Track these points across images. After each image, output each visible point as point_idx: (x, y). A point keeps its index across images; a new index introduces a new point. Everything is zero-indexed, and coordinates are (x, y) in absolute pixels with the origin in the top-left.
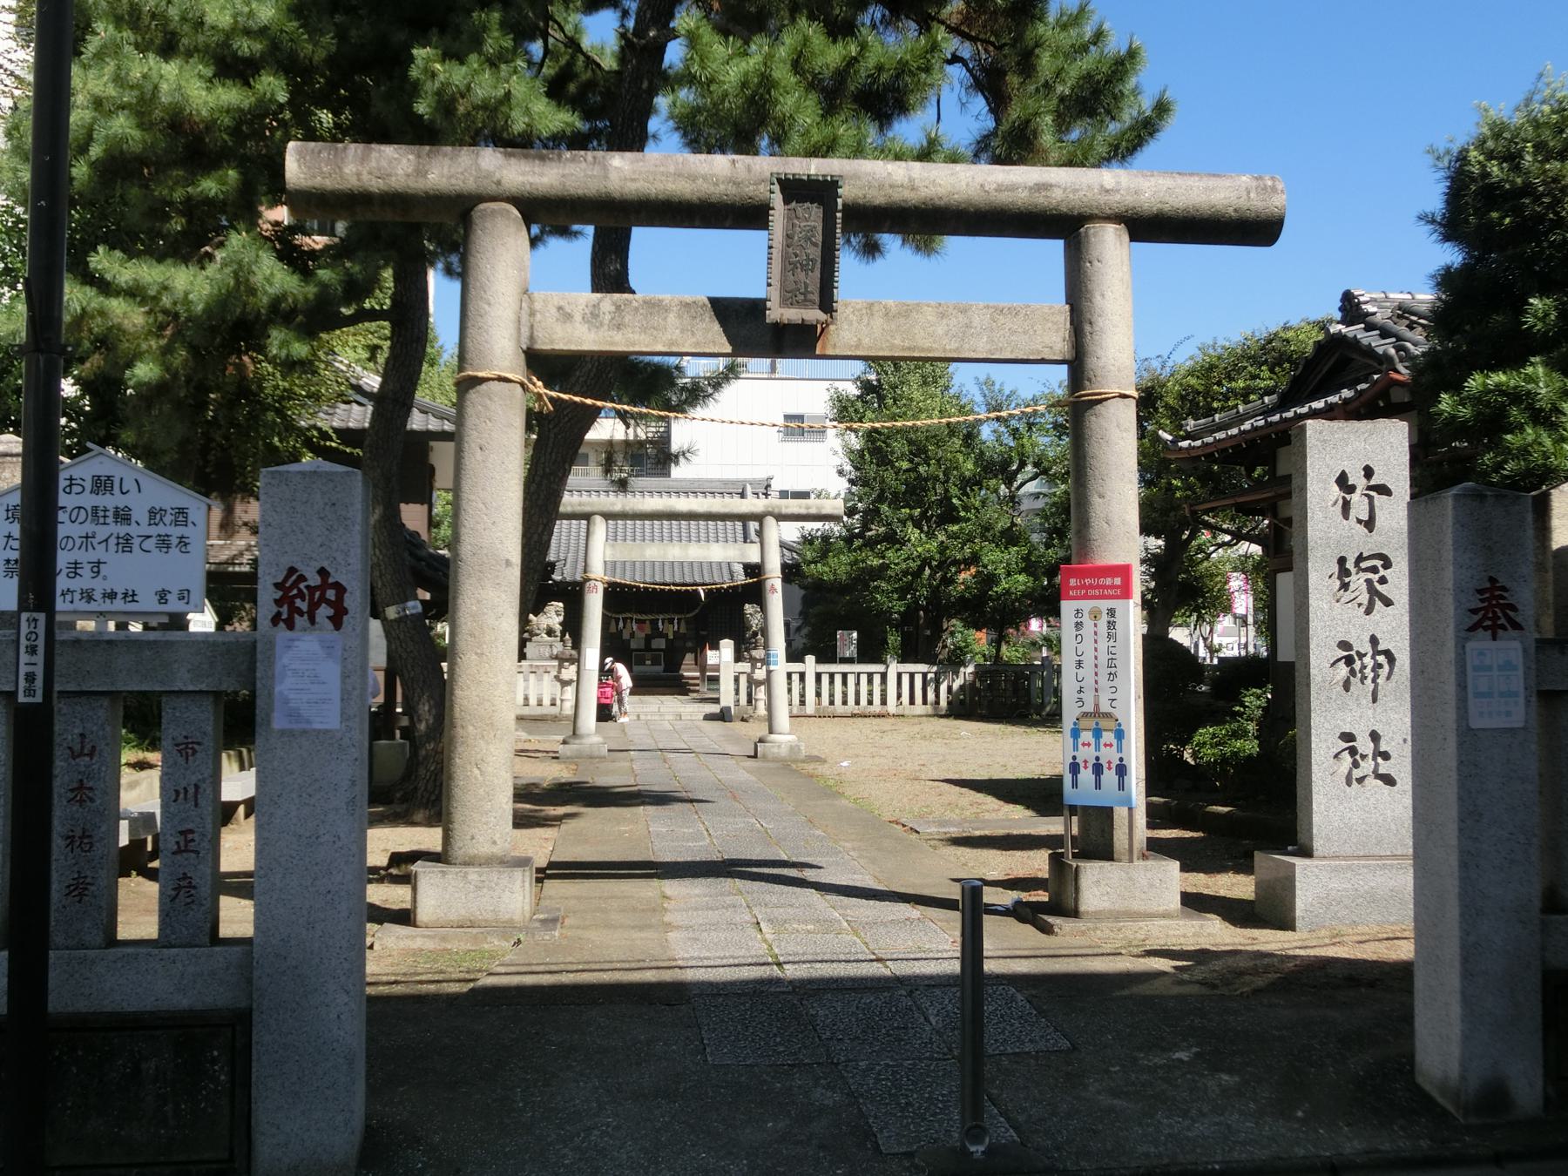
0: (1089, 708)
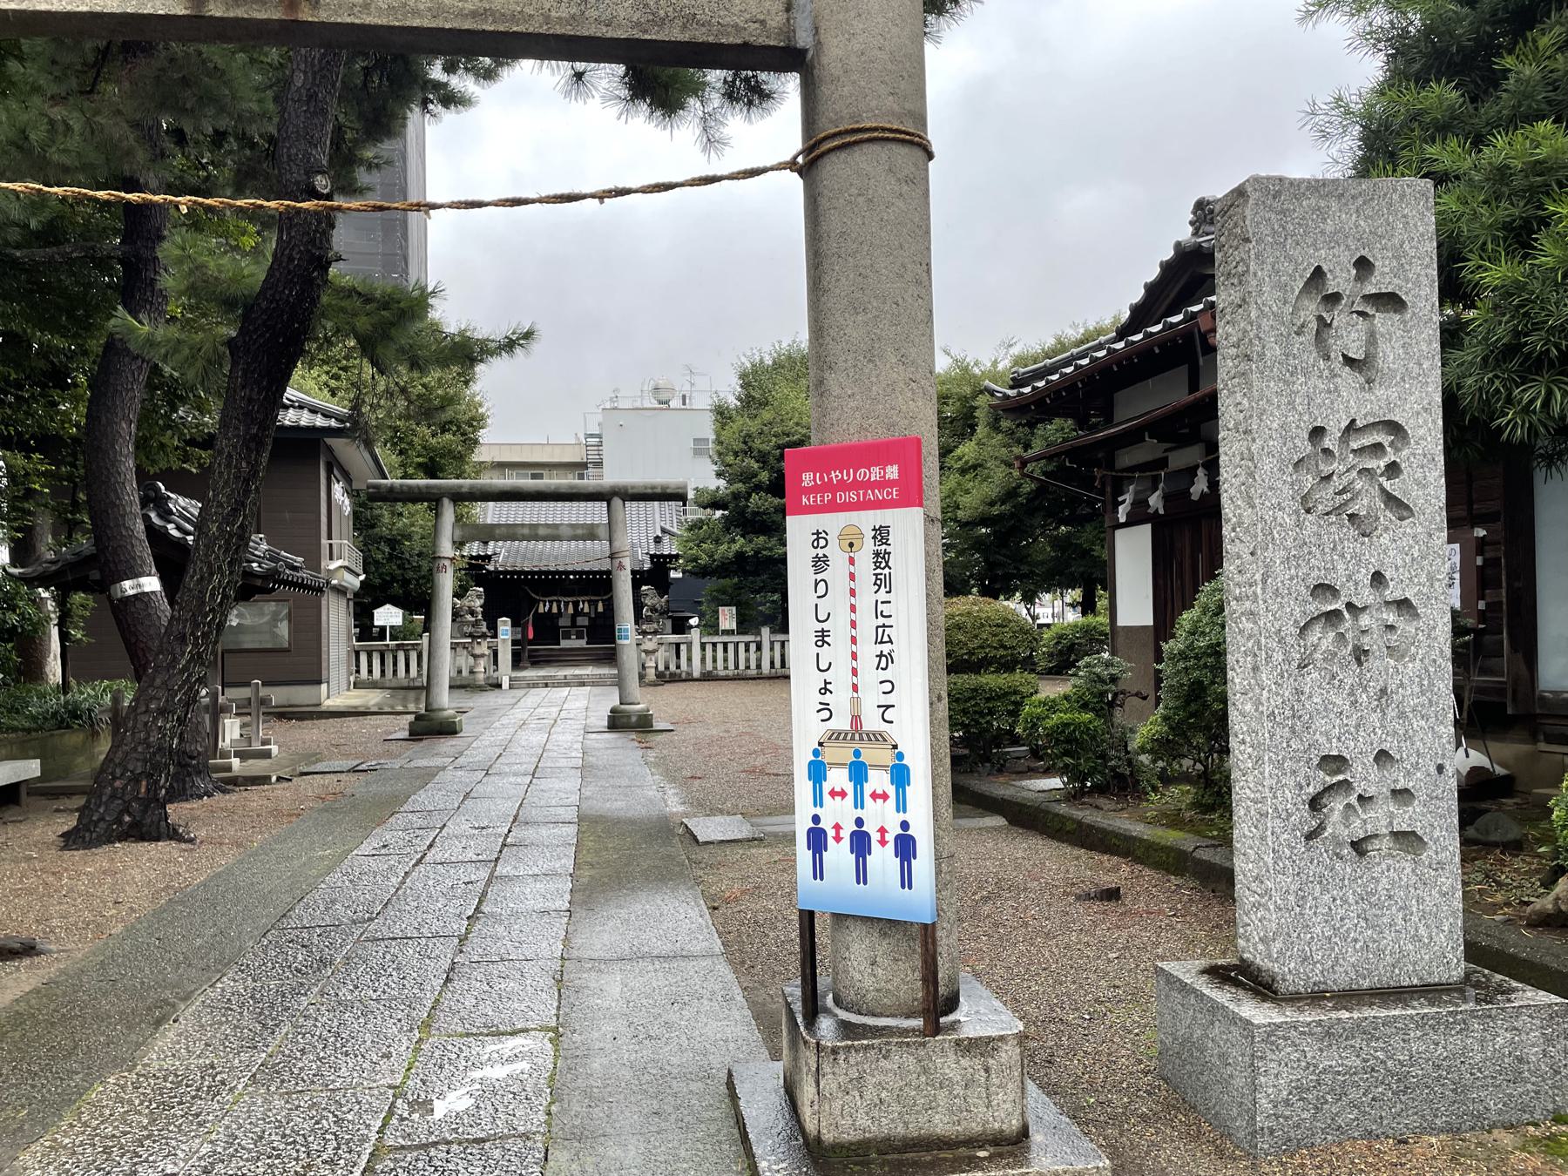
0: (842, 723)
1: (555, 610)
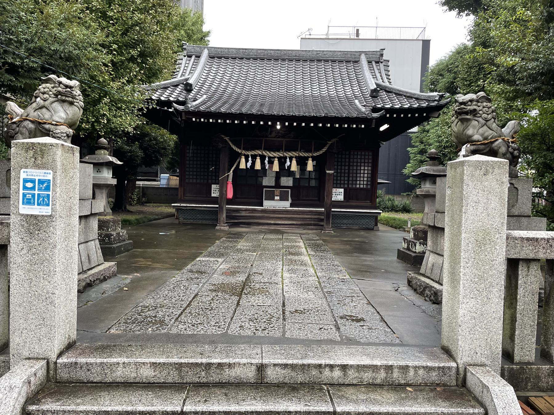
1: (258, 166)
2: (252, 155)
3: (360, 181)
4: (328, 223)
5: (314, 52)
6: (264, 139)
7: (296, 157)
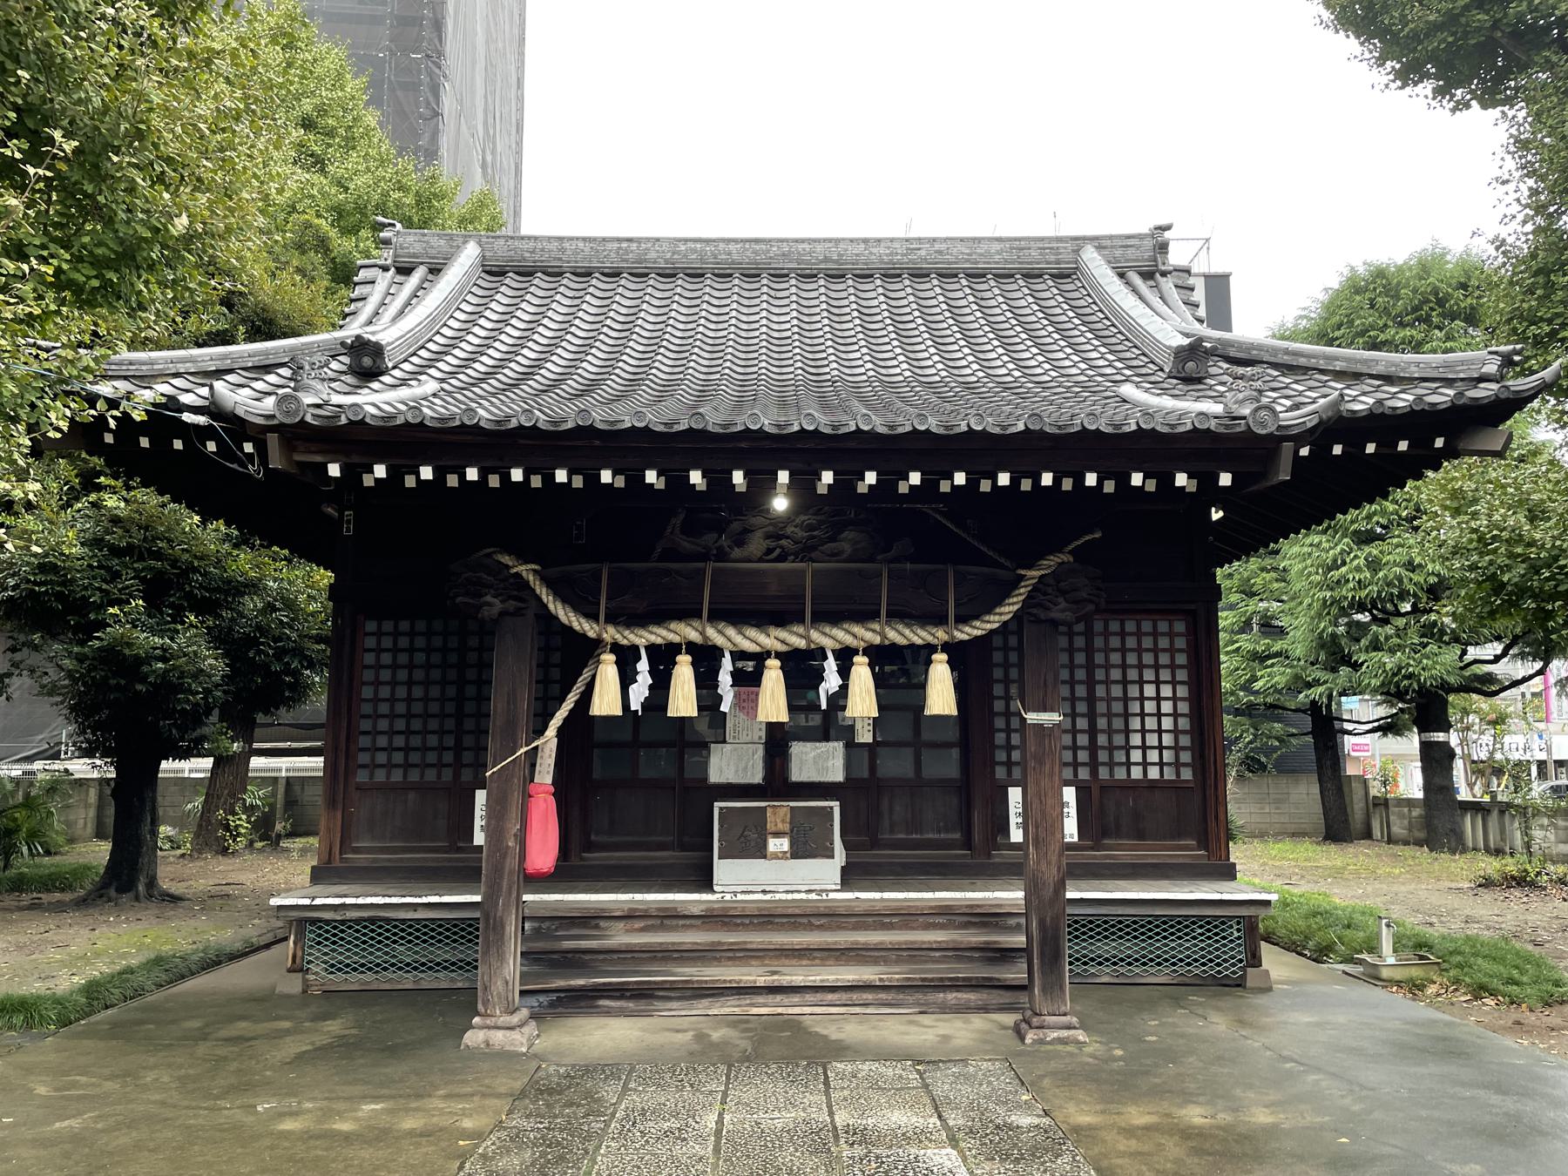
1: (683, 700)
2: (651, 649)
3: (1160, 748)
4: (1053, 986)
5: (896, 245)
6: (710, 567)
7: (947, 647)
